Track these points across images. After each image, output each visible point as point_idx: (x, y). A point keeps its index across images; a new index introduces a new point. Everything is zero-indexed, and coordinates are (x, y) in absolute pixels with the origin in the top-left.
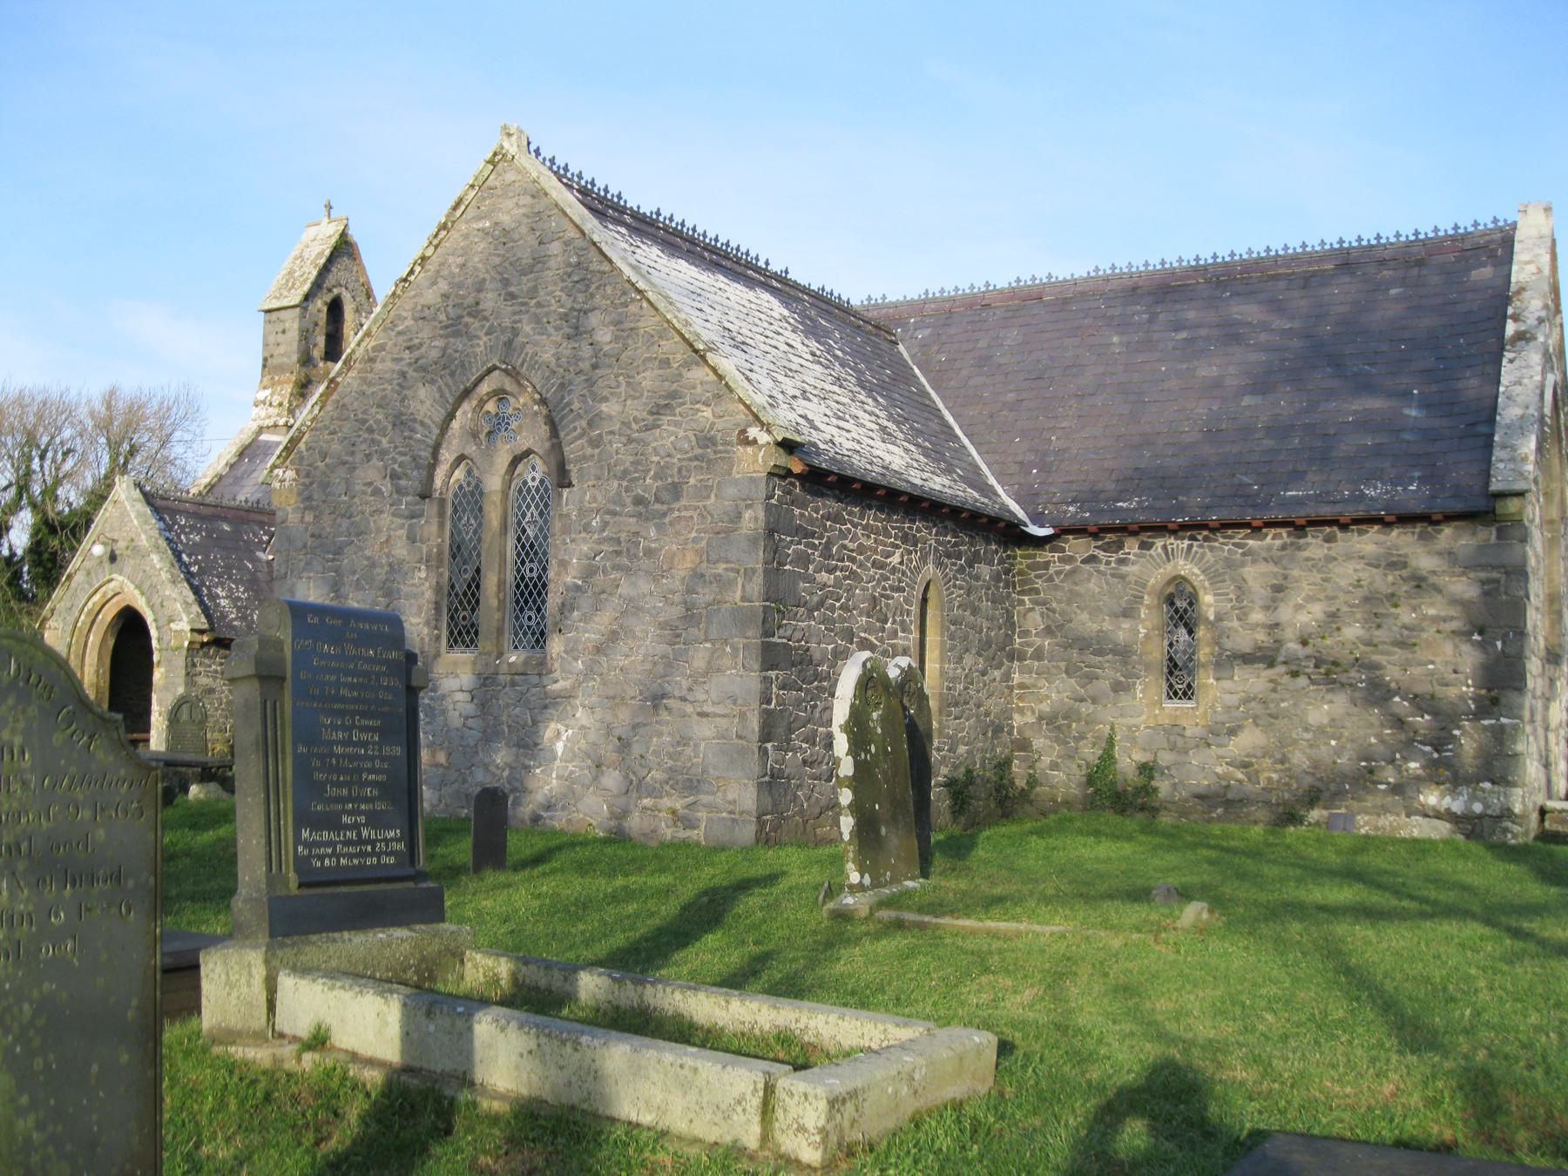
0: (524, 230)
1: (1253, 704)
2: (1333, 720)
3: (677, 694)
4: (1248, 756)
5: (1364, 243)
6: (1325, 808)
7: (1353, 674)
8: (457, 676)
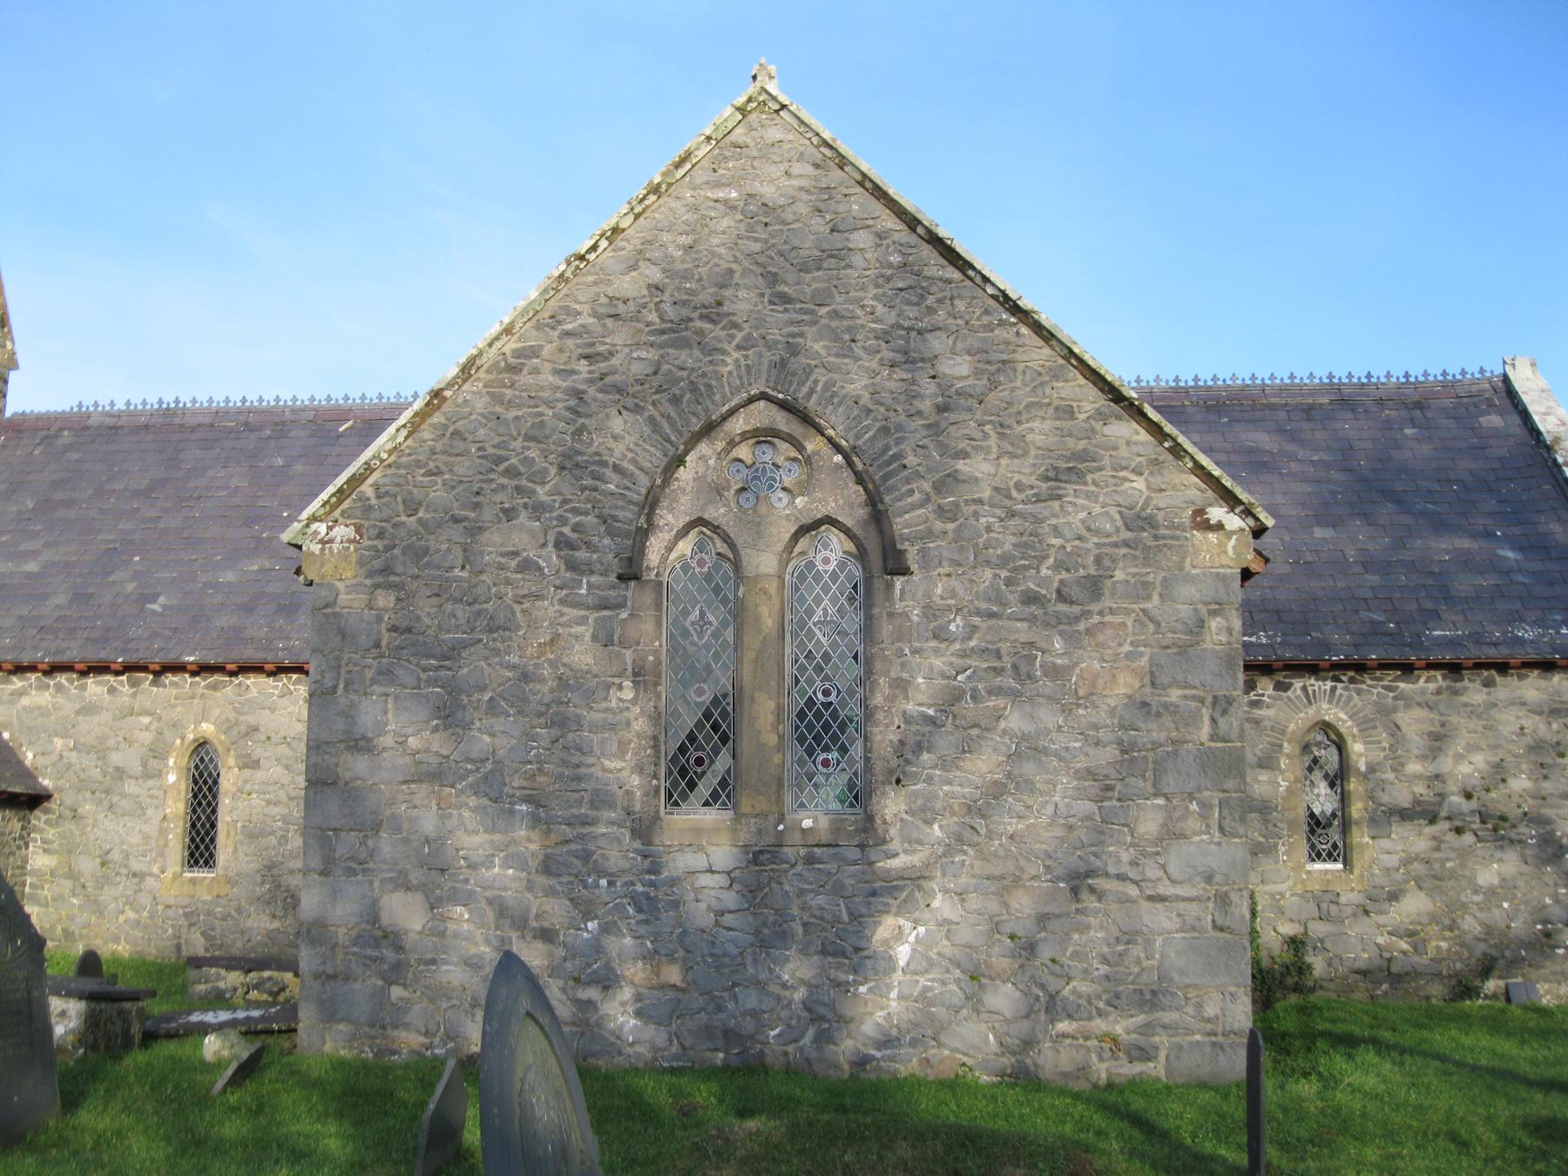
0: (802, 208)
1: (1415, 865)
2: (1504, 880)
3: (1112, 870)
4: (1412, 923)
5: (1355, 380)
6: (1500, 978)
7: (1523, 829)
8: (701, 849)
